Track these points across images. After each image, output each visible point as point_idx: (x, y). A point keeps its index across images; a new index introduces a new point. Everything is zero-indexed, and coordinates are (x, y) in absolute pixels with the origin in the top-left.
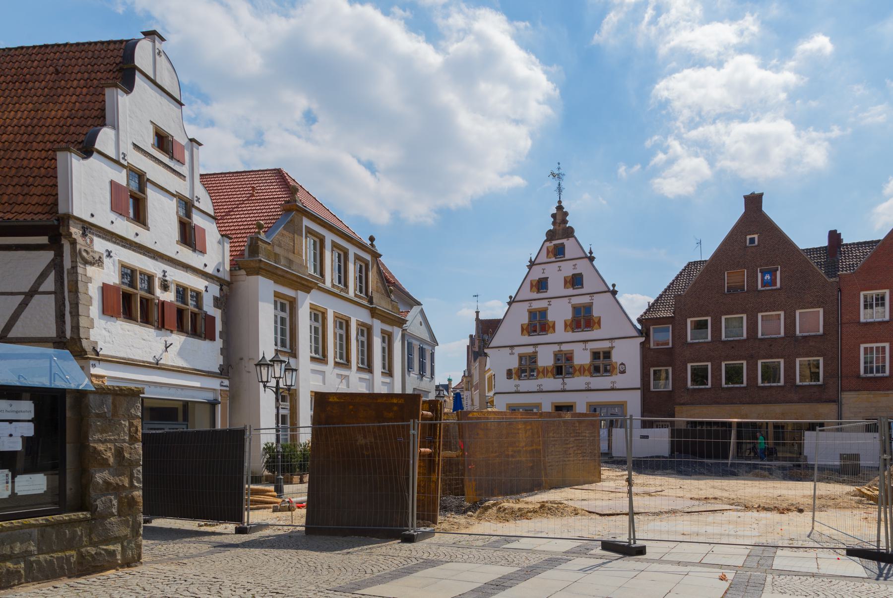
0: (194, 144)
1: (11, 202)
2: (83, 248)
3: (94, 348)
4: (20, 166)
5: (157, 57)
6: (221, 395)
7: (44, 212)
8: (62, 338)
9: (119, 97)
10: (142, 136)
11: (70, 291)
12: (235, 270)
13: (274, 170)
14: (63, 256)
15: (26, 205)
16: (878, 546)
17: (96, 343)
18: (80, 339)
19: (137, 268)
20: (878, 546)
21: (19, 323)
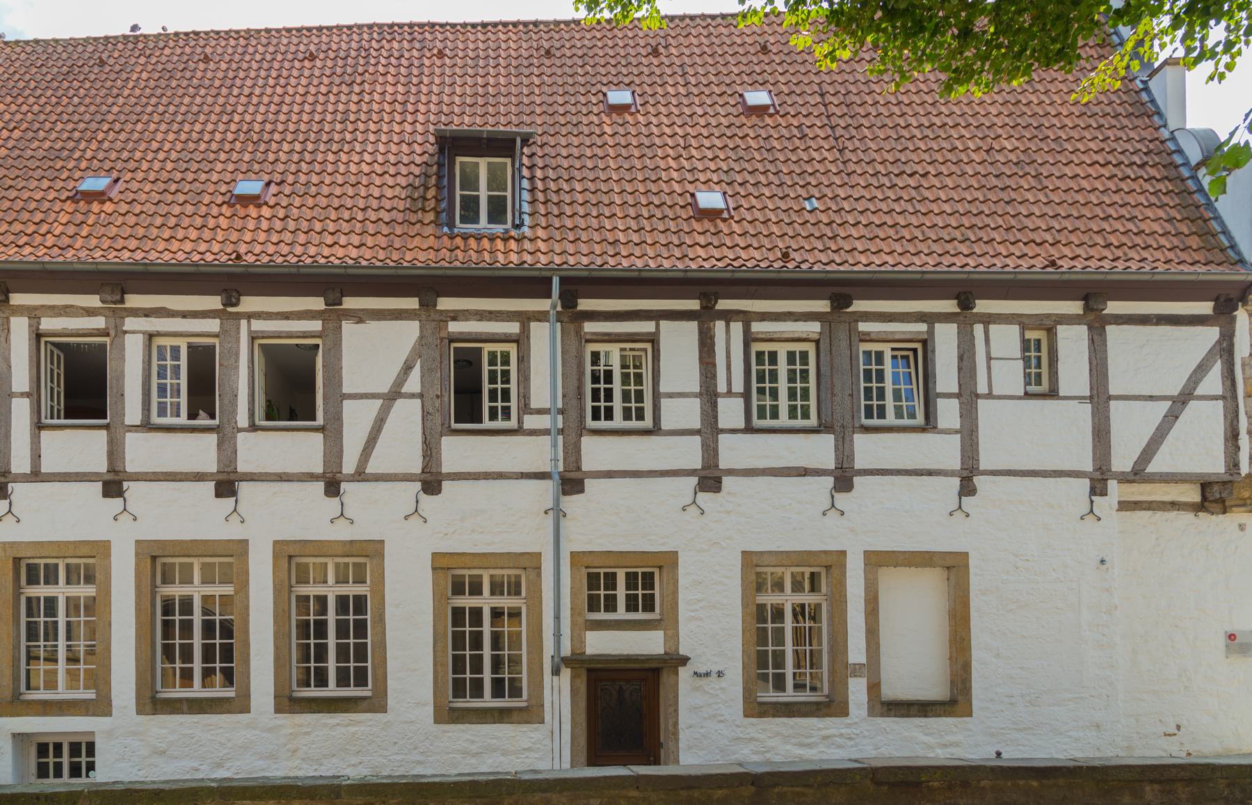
8: (1235, 476)
16: (728, 326)
20: (728, 326)
21: (1165, 448)
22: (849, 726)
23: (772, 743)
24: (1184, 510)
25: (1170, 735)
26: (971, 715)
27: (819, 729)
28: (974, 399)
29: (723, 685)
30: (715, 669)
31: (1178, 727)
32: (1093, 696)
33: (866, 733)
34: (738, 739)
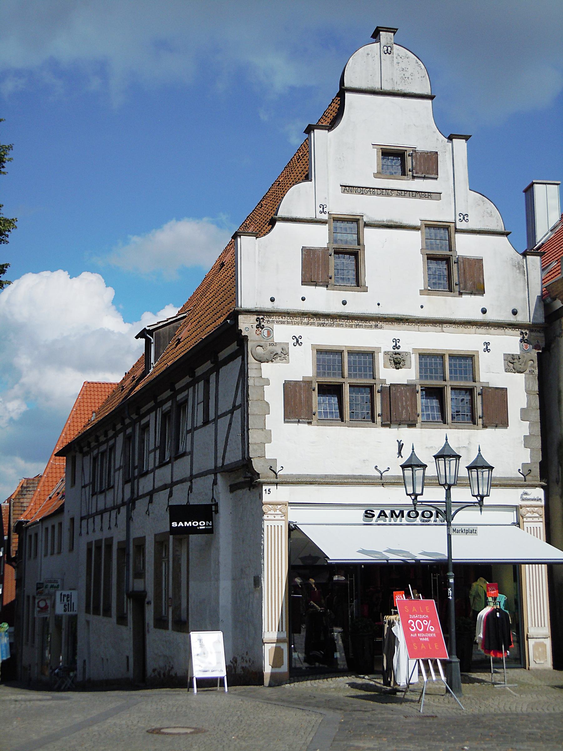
2: (256, 343)
19: (343, 349)
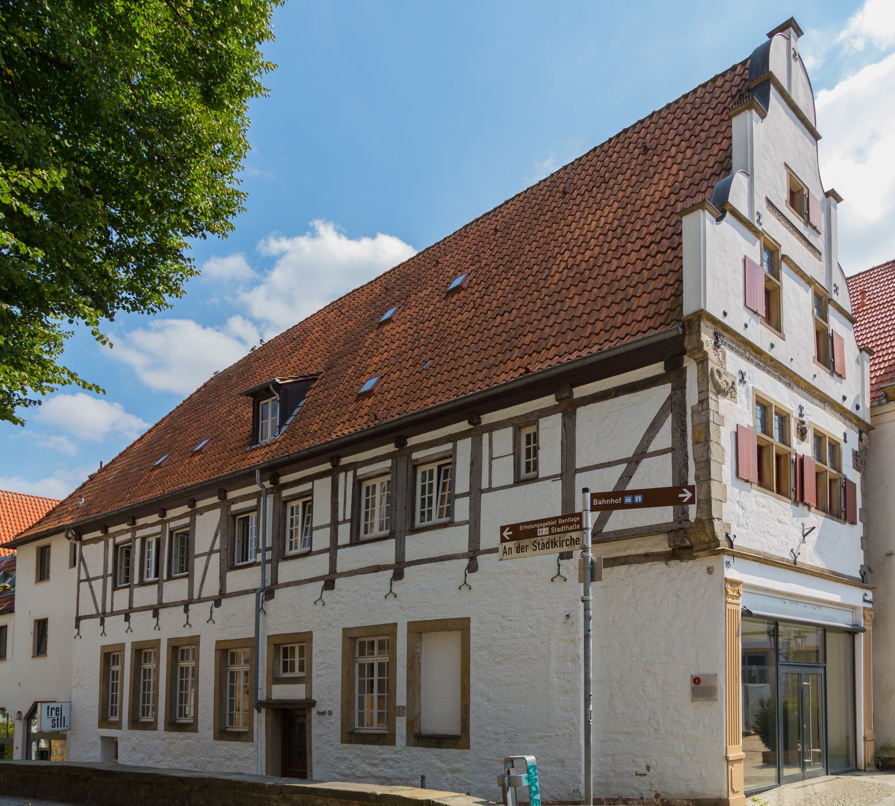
0: (831, 199)
1: (608, 328)
3: (727, 535)
4: (614, 278)
5: (793, 61)
6: (865, 618)
7: (657, 325)
8: (683, 523)
9: (754, 123)
10: (775, 188)
11: (696, 442)
12: (880, 404)
13: (887, 264)
14: (685, 388)
15: (629, 325)
17: (729, 526)
18: (711, 519)
22: (396, 752)
23: (356, 762)
24: (657, 560)
25: (641, 775)
26: (469, 748)
27: (380, 754)
28: (479, 494)
29: (332, 720)
30: (329, 709)
31: (648, 768)
32: (558, 736)
33: (406, 758)
34: (339, 758)
